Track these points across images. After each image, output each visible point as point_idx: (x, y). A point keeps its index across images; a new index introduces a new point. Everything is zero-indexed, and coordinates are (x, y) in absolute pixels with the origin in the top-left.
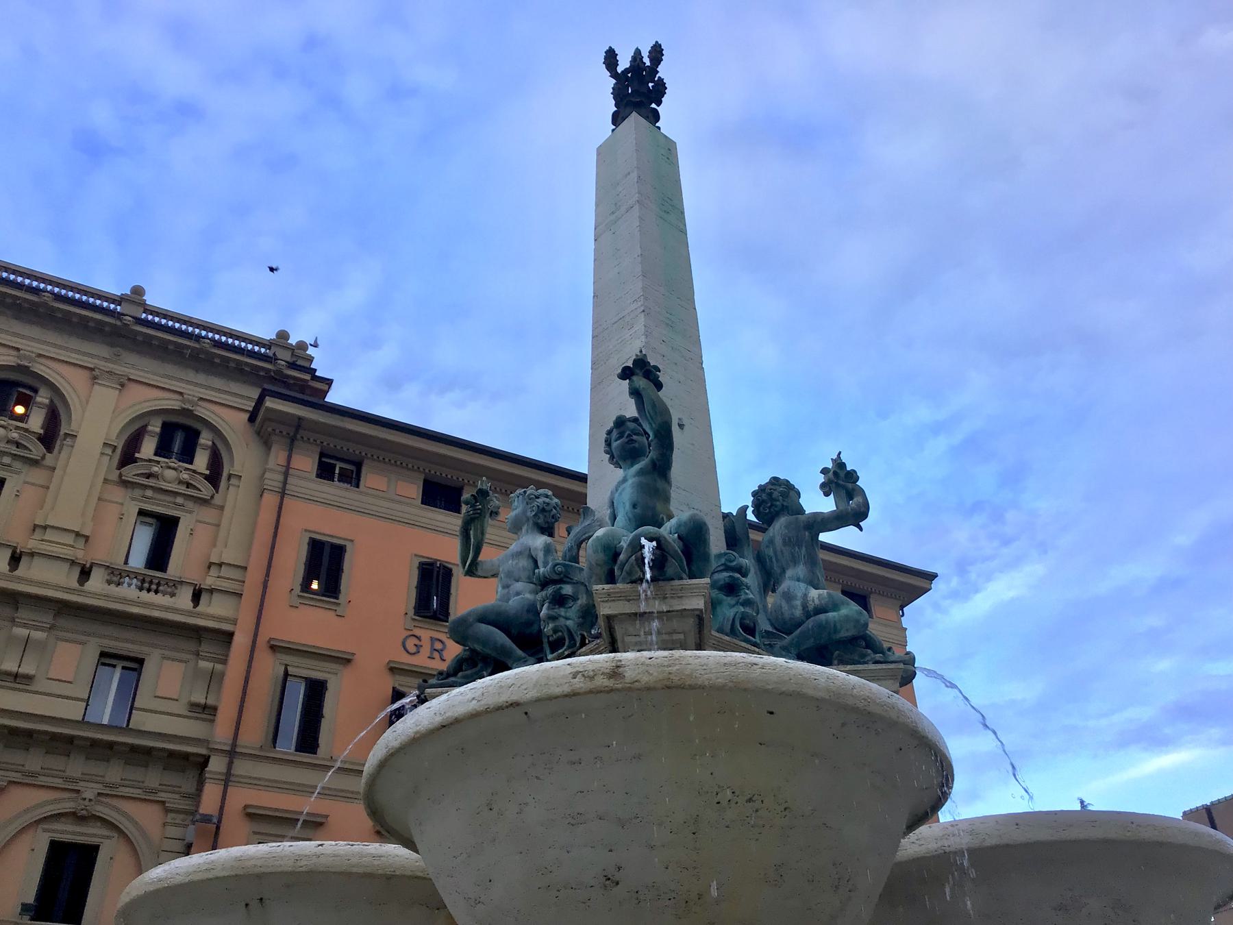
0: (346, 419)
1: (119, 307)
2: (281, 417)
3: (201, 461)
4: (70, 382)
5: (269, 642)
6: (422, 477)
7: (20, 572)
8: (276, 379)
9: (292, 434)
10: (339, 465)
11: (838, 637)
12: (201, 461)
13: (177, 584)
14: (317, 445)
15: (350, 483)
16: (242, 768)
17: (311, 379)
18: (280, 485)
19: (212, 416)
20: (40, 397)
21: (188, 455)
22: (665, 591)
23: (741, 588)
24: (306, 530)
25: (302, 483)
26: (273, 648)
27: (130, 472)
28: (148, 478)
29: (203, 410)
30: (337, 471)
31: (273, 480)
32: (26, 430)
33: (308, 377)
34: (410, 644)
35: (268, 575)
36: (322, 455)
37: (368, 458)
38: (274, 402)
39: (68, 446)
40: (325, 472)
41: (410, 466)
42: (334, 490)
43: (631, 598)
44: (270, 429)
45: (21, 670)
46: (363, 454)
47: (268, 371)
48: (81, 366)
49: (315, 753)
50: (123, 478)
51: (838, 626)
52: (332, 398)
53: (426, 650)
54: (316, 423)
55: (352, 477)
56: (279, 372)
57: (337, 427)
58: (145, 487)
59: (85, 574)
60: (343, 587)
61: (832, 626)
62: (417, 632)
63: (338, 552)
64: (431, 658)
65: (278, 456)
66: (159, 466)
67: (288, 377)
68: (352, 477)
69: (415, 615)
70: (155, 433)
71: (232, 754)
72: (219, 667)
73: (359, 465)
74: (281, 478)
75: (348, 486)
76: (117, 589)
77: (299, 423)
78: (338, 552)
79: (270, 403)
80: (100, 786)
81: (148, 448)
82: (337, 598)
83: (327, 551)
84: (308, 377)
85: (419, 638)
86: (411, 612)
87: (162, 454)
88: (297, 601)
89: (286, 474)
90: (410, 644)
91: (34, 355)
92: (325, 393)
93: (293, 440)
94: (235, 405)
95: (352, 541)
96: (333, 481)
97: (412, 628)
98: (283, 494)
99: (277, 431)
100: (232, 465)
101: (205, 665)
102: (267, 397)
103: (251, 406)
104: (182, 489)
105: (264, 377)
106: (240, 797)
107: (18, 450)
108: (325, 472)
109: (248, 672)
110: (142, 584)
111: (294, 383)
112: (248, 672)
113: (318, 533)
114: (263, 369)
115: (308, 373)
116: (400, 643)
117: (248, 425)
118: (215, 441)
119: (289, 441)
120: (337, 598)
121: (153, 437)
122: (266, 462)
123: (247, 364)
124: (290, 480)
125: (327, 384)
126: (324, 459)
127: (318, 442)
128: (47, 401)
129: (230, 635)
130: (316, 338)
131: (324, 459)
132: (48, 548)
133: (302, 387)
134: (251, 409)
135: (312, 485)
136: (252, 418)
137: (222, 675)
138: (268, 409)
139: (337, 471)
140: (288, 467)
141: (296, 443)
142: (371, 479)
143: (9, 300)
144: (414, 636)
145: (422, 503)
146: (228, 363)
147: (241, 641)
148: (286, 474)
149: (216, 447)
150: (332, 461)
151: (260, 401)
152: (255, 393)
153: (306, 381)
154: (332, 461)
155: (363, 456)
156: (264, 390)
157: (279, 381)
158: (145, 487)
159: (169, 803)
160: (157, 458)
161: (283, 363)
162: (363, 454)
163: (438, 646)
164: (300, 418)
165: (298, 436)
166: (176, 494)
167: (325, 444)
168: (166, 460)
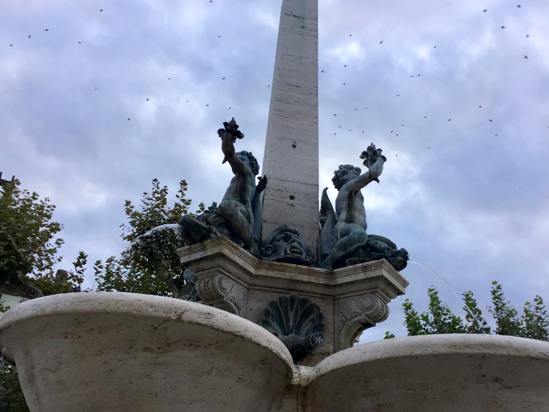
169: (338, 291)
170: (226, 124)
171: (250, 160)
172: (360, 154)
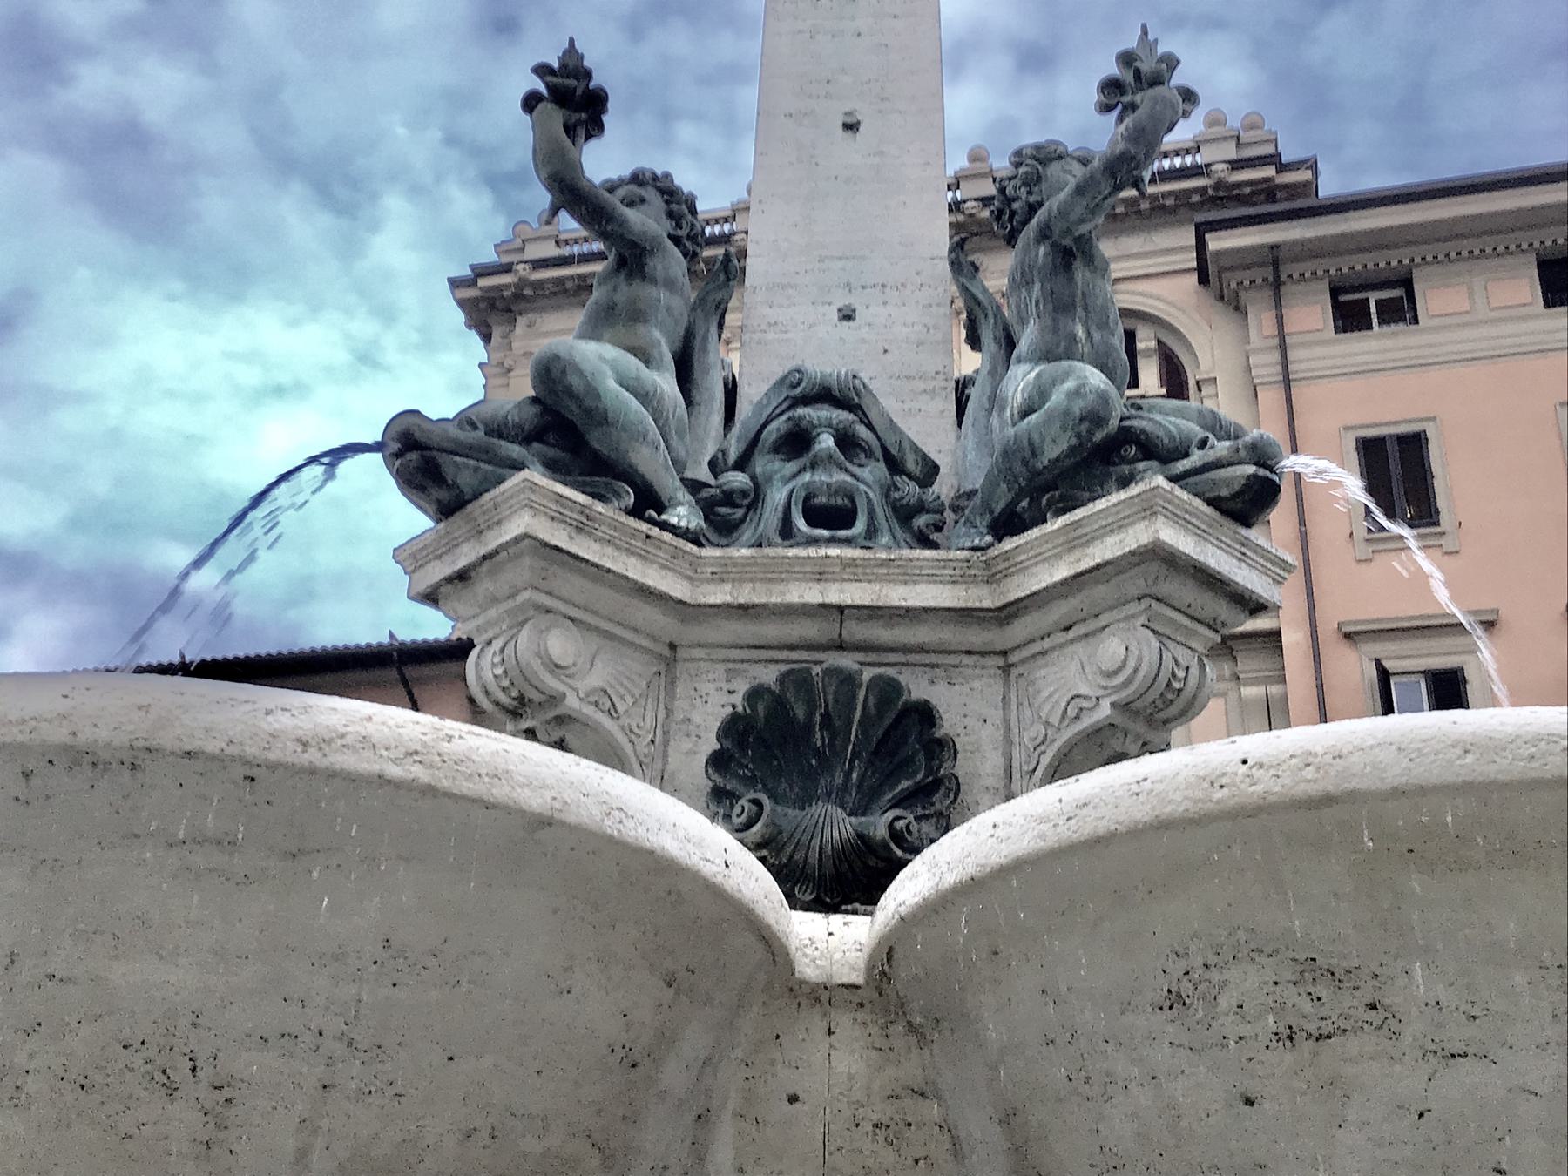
0: (1352, 214)
1: (958, 193)
2: (1243, 259)
5: (1339, 629)
6: (1532, 259)
8: (1221, 198)
9: (1271, 279)
10: (1373, 297)
11: (1044, 460)
14: (1261, 287)
15: (1402, 319)
17: (1277, 173)
18: (1279, 368)
19: (1140, 299)
20: (1141, 341)
22: (476, 520)
23: (814, 433)
24: (1347, 428)
25: (1319, 351)
29: (1127, 297)
30: (1373, 309)
31: (1266, 365)
33: (1270, 171)
35: (1302, 521)
36: (1335, 292)
37: (1418, 266)
38: (1219, 239)
39: (1210, 397)
40: (1350, 318)
41: (1501, 249)
42: (1377, 343)
43: (440, 552)
44: (1233, 285)
46: (1406, 262)
47: (1202, 191)
48: (1164, 274)
51: (1036, 438)
52: (1329, 187)
54: (1302, 243)
55: (1401, 311)
56: (1219, 185)
57: (1549, 206)
60: (1441, 503)
61: (1025, 442)
63: (1413, 444)
65: (1261, 321)
67: (1239, 185)
68: (1401, 311)
72: (1274, 690)
73: (1407, 283)
74: (1276, 356)
75: (1401, 326)
77: (1274, 257)
78: (1413, 444)
79: (1217, 242)
82: (1436, 524)
84: (1270, 171)
88: (1364, 551)
89: (1283, 348)
92: (1310, 187)
93: (1277, 285)
94: (1177, 267)
95: (1434, 419)
96: (1370, 327)
97: (1371, 556)
98: (1287, 382)
99: (1246, 283)
100: (1198, 367)
101: (1251, 692)
102: (1207, 236)
105: (1202, 203)
108: (1350, 318)
109: (1320, 687)
111: (1252, 192)
112: (1320, 687)
113: (1368, 426)
114: (1196, 190)
115: (1269, 164)
117: (1201, 289)
118: (1164, 340)
119: (1269, 293)
120: (1436, 524)
122: (1246, 340)
123: (1165, 195)
124: (1291, 356)
125: (1307, 168)
126: (1342, 298)
127: (1320, 273)
128: (1153, 344)
129: (1275, 635)
131: (1342, 298)
133: (1268, 191)
134: (1195, 264)
135: (1340, 349)
136: (1203, 279)
137: (1285, 699)
138: (1218, 253)
139: (1373, 309)
140: (1282, 337)
141: (1283, 289)
142: (1432, 298)
143: (1196, 198)
145: (1547, 305)
146: (564, 284)
147: (1294, 639)
148: (1283, 348)
149: (1165, 345)
150: (1357, 296)
151: (1201, 245)
152: (1190, 238)
153: (1267, 180)
154: (1357, 296)
155: (1408, 265)
156: (1198, 227)
157: (1229, 198)
162: (1406, 262)
164: (1274, 247)
165: (1283, 278)
167: (1333, 272)
169: (1020, 629)
170: (542, 70)
171: (667, 202)
172: (1094, 96)
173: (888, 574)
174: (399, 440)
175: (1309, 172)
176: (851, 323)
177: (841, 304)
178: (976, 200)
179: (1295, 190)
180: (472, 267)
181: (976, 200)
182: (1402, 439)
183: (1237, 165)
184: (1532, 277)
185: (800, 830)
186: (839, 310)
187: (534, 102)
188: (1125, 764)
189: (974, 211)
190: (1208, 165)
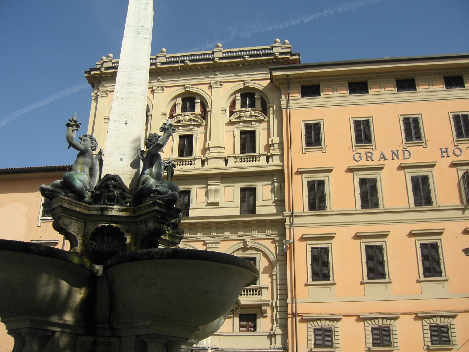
3: (198, 109)
4: (203, 90)
7: (205, 166)
12: (198, 109)
13: (260, 156)
16: (297, 221)
21: (193, 109)
26: (299, 173)
27: (233, 118)
28: (240, 118)
32: (195, 114)
33: (289, 56)
34: (357, 157)
38: (275, 72)
45: (215, 201)
49: (326, 210)
50: (231, 121)
52: (303, 62)
53: (364, 158)
58: (239, 122)
59: (226, 161)
62: (358, 151)
64: (367, 161)
66: (243, 112)
69: (406, 141)
70: (199, 102)
71: (292, 216)
76: (244, 163)
79: (274, 74)
80: (250, 236)
81: (238, 106)
83: (411, 121)
85: (360, 154)
86: (404, 141)
87: (244, 107)
90: (357, 157)
91: (250, 81)
92: (299, 61)
103: (269, 76)
104: (253, 118)
106: (298, 233)
107: (255, 118)
110: (241, 160)
116: (412, 154)
118: (262, 95)
121: (258, 100)
125: (297, 56)
128: (259, 97)
130: (398, 159)
132: (212, 155)
134: (269, 77)
141: (290, 86)
144: (357, 153)
158: (239, 122)
159: (206, 240)
160: (242, 109)
161: (217, 59)
163: (369, 155)
164: (288, 75)
166: (251, 121)
168: (245, 109)
173: (190, 129)
174: (278, 137)
175: (298, 57)
176: (122, 161)
177: (121, 158)
178: (218, 58)
179: (294, 61)
180: (90, 69)
181: (218, 58)
182: (364, 121)
183: (281, 54)
184: (394, 85)
185: (278, 204)
186: (120, 159)
187: (54, 243)
188: (173, 135)
189: (217, 61)
190: (274, 53)
